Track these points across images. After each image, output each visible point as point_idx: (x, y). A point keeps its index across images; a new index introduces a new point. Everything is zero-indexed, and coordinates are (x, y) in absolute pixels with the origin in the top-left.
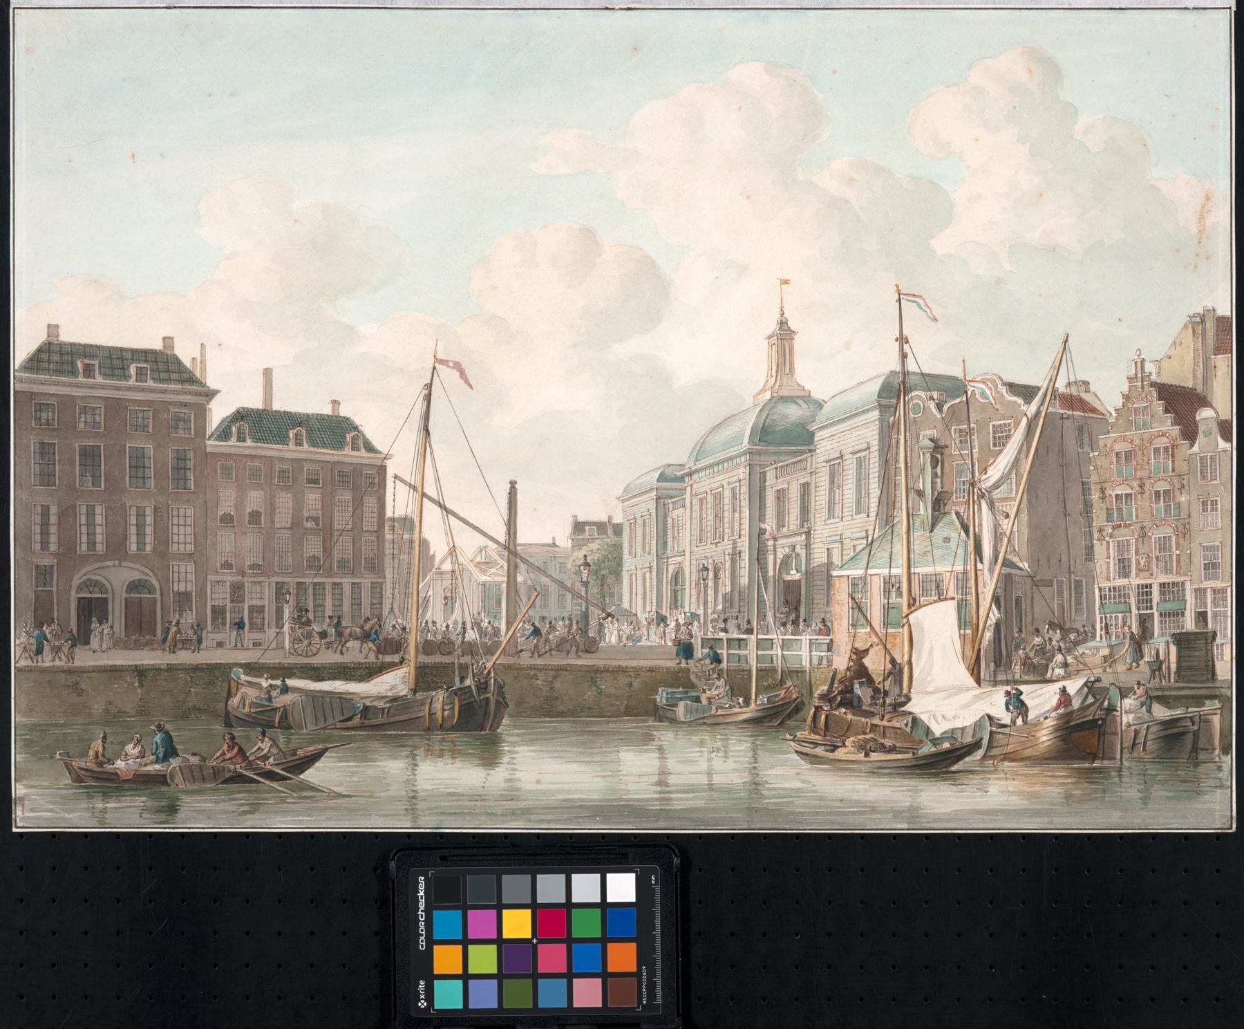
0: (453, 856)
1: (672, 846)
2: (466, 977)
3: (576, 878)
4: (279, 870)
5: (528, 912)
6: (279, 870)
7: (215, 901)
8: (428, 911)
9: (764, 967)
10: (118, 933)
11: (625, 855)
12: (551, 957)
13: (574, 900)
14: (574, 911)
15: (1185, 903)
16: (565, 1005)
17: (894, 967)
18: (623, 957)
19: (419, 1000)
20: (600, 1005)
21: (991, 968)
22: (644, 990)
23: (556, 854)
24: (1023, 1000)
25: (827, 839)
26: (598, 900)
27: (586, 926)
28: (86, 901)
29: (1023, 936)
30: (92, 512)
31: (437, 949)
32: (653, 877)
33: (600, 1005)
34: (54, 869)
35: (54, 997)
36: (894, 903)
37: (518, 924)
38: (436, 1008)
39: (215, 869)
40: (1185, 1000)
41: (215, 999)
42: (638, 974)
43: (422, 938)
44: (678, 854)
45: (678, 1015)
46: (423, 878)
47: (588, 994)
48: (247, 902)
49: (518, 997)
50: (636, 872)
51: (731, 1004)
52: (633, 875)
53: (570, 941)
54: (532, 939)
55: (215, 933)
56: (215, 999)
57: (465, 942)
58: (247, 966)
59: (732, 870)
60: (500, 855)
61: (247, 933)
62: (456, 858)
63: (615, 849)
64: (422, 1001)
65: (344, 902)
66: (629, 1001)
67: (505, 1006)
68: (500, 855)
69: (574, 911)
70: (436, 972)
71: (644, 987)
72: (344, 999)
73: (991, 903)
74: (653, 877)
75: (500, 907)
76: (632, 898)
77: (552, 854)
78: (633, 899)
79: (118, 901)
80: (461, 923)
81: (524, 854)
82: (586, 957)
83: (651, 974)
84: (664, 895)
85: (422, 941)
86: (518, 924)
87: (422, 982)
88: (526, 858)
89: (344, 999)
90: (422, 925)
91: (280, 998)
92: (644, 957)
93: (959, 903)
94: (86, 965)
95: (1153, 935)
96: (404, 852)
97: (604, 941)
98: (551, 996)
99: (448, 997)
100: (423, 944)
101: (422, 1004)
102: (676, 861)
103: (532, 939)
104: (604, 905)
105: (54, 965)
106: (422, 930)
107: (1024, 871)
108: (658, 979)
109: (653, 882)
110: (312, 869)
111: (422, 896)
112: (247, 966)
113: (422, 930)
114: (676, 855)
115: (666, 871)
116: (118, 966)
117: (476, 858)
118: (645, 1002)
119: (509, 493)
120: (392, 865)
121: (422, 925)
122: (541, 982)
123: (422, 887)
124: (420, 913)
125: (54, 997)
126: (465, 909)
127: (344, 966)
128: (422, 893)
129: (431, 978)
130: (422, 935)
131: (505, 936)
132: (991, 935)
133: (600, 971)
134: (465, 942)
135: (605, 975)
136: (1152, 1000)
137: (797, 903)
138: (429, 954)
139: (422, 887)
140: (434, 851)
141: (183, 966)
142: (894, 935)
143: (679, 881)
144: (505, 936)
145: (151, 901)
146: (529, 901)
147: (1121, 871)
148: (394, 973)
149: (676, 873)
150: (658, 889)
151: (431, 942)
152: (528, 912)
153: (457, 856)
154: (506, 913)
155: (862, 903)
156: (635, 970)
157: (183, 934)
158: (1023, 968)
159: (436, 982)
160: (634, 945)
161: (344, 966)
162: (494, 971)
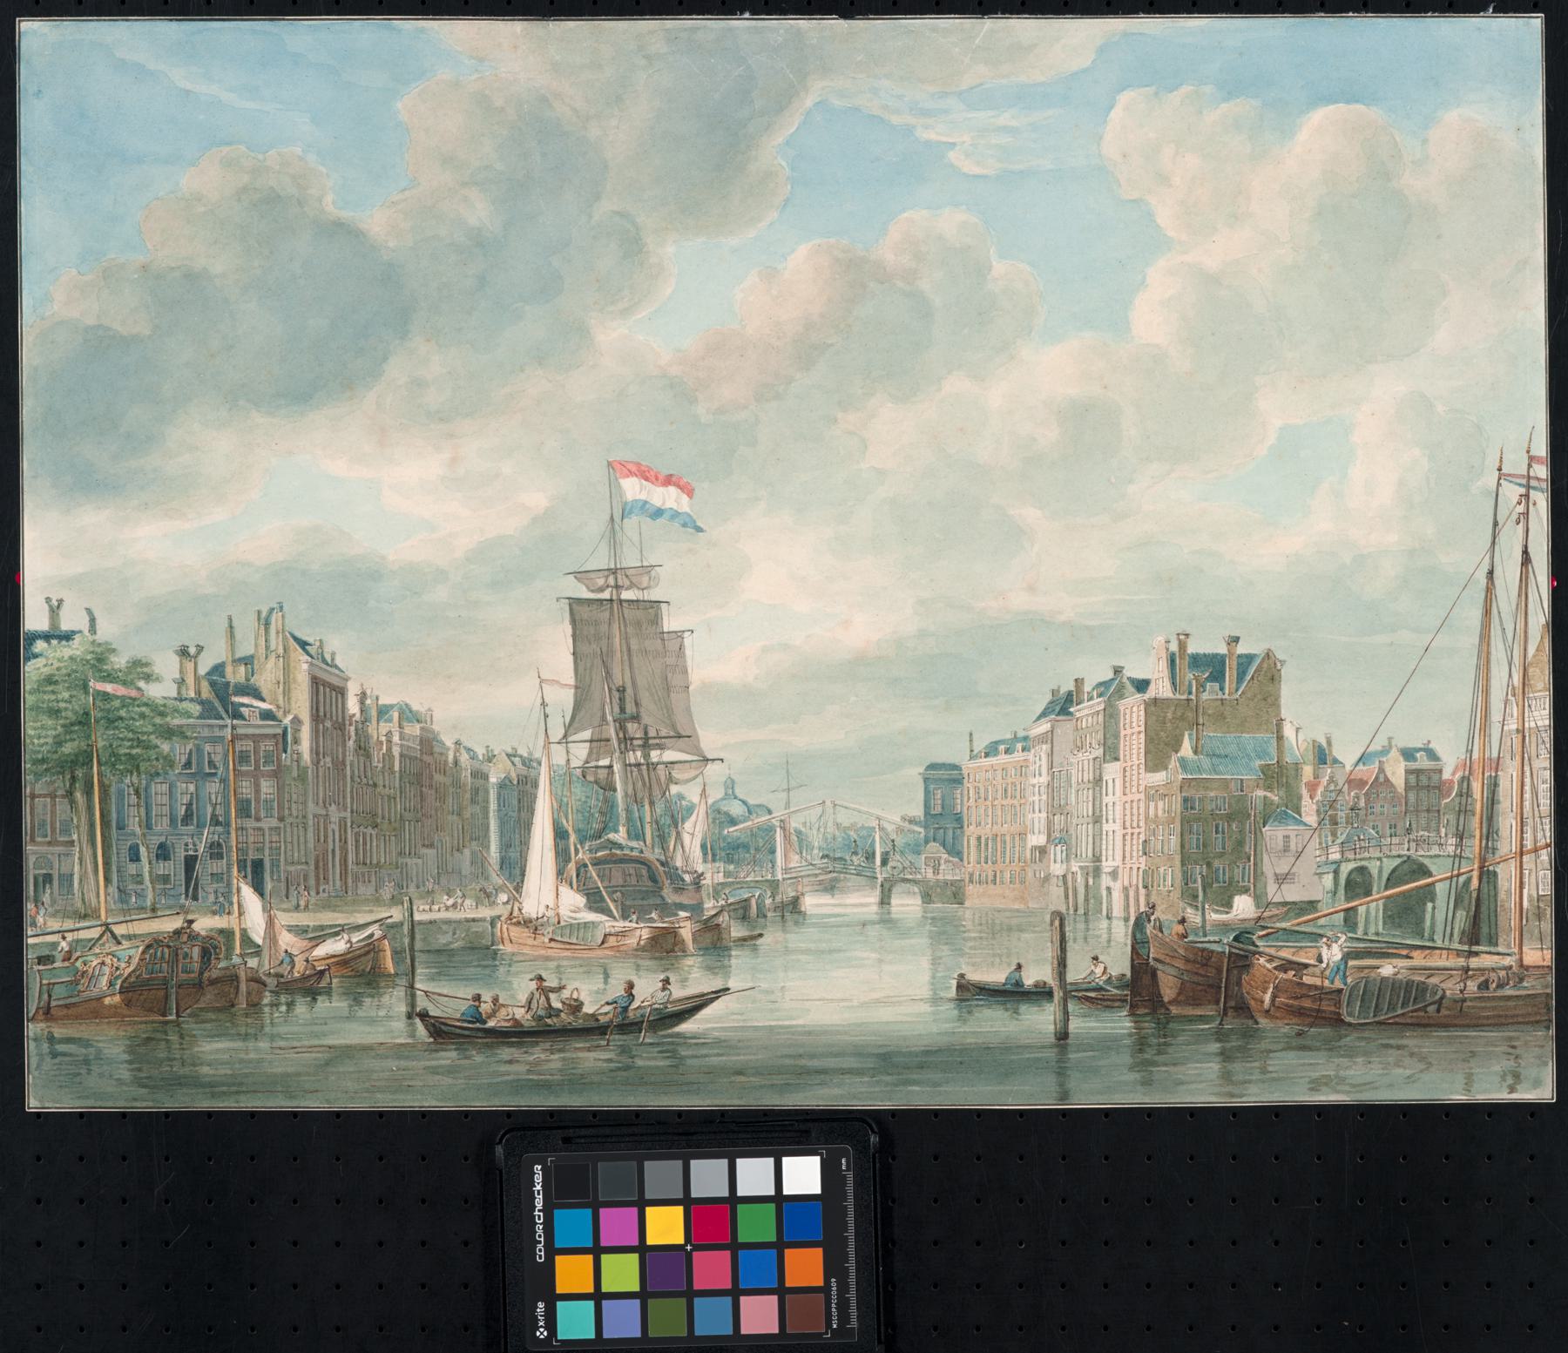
0: (579, 1137)
1: (870, 1121)
2: (598, 1296)
3: (741, 1163)
4: (338, 1159)
5: (679, 1210)
6: (338, 1159)
7: (252, 1202)
8: (548, 1210)
9: (978, 1286)
10: (124, 1244)
11: (807, 1132)
12: (711, 1268)
13: (740, 1193)
14: (740, 1207)
15: (1532, 1200)
16: (729, 1331)
17: (1148, 1286)
18: (806, 1267)
19: (538, 1328)
20: (776, 1331)
21: (1276, 1286)
22: (834, 1310)
23: (715, 1133)
24: (1318, 1328)
25: (1061, 1117)
26: (772, 1192)
27: (756, 1226)
28: (81, 1202)
29: (1319, 1243)
30: (579, 691)
31: (560, 1260)
32: (843, 1161)
33: (776, 1331)
34: (39, 1159)
35: (39, 1329)
36: (1149, 1201)
37: (666, 1226)
38: (559, 1338)
39: (252, 1159)
40: (1531, 1327)
41: (253, 1330)
42: (826, 1289)
43: (540, 1246)
44: (876, 1130)
45: (880, 1342)
46: (539, 1167)
47: (760, 1316)
48: (295, 1202)
49: (668, 1321)
50: (821, 1155)
51: (935, 1334)
52: (817, 1159)
53: (735, 1247)
54: (686, 1244)
55: (252, 1244)
56: (253, 1330)
57: (597, 1251)
58: (295, 1287)
59: (936, 1158)
60: (642, 1135)
61: (295, 1244)
62: (583, 1141)
63: (792, 1125)
64: (542, 1330)
65: (423, 1201)
66: (811, 1324)
67: (651, 1334)
68: (642, 1135)
69: (740, 1207)
70: (559, 1290)
71: (833, 1305)
72: (423, 1330)
73: (1276, 1201)
74: (843, 1161)
75: (642, 1204)
76: (815, 1188)
77: (710, 1133)
78: (817, 1190)
79: (124, 1201)
80: (591, 1222)
81: (674, 1134)
82: (756, 1268)
83: (843, 1288)
84: (858, 1184)
85: (540, 1250)
86: (666, 1226)
87: (541, 1305)
88: (676, 1138)
89: (423, 1330)
90: (539, 1229)
91: (338, 1329)
92: (833, 1267)
93: (1234, 1201)
94: (81, 1287)
95: (1489, 1243)
96: (515, 1133)
97: (780, 1246)
98: (711, 1320)
99: (575, 1322)
100: (541, 1255)
101: (542, 1333)
102: (874, 1139)
103: (686, 1244)
104: (779, 1198)
105: (39, 1287)
106: (540, 1236)
107: (1319, 1158)
108: (852, 1295)
109: (844, 1167)
110: (381, 1159)
111: (539, 1191)
112: (295, 1287)
113: (540, 1236)
114: (873, 1132)
115: (861, 1152)
116: (124, 1287)
117: (609, 1140)
118: (835, 1326)
119: (574, 654)
120: (499, 1150)
121: (539, 1229)
122: (697, 1301)
123: (538, 1178)
124: (536, 1213)
125: (39, 1329)
126: (596, 1207)
127: (423, 1286)
128: (539, 1187)
129: (552, 1298)
130: (540, 1242)
131: (650, 1242)
132: (1276, 1243)
133: (776, 1286)
134: (597, 1251)
135: (781, 1291)
136: (1488, 1328)
137: (1021, 1201)
138: (550, 1266)
139: (538, 1178)
140: (554, 1131)
141: (210, 1287)
142: (1149, 1243)
143: (878, 1165)
144: (650, 1242)
145: (167, 1202)
146: (680, 1196)
147: (1447, 1158)
148: (504, 1293)
149: (874, 1155)
150: (850, 1176)
151: (552, 1251)
152: (679, 1210)
153: (584, 1137)
154: (651, 1212)
155: (1106, 1201)
156: (821, 1283)
157: (210, 1245)
158: (1319, 1285)
159: (559, 1304)
160: (819, 1252)
161: (423, 1286)
162: (636, 1288)
